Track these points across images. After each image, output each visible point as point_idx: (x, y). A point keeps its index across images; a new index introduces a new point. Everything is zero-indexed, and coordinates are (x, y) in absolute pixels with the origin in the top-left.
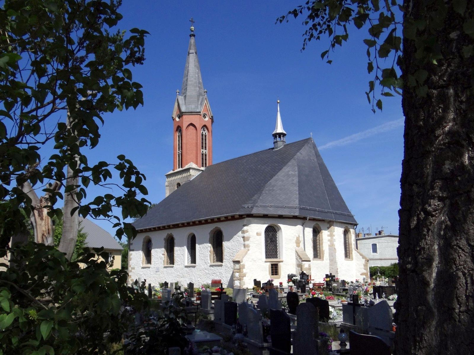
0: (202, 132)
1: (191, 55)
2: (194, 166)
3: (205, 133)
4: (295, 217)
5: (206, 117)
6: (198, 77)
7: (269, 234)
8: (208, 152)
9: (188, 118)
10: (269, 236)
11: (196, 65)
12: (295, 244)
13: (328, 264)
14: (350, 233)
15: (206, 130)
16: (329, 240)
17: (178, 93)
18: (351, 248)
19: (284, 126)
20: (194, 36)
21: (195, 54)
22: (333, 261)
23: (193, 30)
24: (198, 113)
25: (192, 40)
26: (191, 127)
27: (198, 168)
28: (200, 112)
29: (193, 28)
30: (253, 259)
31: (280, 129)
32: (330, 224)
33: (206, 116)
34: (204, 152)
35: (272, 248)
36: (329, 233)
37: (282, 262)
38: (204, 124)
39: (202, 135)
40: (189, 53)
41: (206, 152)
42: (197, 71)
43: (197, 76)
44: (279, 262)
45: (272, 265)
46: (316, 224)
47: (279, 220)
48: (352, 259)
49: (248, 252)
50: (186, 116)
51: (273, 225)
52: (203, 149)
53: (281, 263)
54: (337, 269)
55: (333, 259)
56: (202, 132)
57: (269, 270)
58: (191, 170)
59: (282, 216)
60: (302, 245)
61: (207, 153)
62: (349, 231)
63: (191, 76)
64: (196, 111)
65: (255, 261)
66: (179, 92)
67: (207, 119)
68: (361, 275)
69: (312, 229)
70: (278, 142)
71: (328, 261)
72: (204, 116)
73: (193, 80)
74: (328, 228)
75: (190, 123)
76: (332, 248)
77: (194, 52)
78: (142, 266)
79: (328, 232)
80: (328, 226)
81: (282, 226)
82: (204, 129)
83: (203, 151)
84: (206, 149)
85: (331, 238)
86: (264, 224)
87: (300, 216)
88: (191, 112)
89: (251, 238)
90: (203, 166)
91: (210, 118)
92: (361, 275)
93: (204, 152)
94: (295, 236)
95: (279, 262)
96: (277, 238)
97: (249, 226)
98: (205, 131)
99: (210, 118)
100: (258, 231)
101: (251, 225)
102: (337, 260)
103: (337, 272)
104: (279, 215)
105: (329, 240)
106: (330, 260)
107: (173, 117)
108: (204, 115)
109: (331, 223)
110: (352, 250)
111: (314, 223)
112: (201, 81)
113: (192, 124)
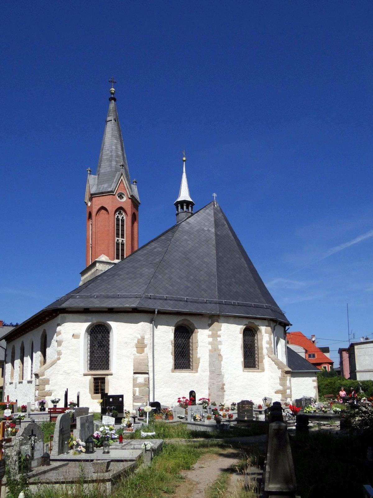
0: (118, 216)
1: (109, 123)
2: (104, 258)
3: (123, 217)
4: (135, 311)
5: (123, 197)
6: (117, 148)
7: (97, 336)
8: (126, 241)
9: (98, 200)
10: (97, 338)
11: (113, 134)
12: (135, 349)
13: (207, 378)
14: (261, 332)
15: (124, 214)
16: (210, 343)
17: (89, 172)
18: (262, 353)
19: (192, 192)
20: (115, 99)
21: (113, 121)
22: (216, 372)
23: (113, 92)
24: (111, 193)
25: (112, 104)
26: (103, 211)
27: (110, 261)
28: (112, 192)
29: (113, 89)
30: (65, 372)
31: (184, 195)
32: (211, 319)
33: (124, 196)
34: (120, 241)
35: (99, 353)
36: (210, 333)
37: (112, 375)
38: (119, 206)
39: (118, 220)
40: (107, 122)
41: (123, 241)
42: (116, 141)
43: (114, 147)
44: (107, 375)
45: (95, 379)
46: (183, 320)
47: (109, 315)
48: (263, 370)
49: (58, 362)
50: (96, 198)
51: (252, 327)
52: (118, 235)
53: (109, 377)
54: (224, 385)
55: (215, 370)
56: (116, 216)
57: (90, 387)
58: (97, 264)
59: (180, 312)
60: (148, 350)
61: (125, 242)
62: (258, 329)
63: (107, 148)
64: (107, 191)
65: (68, 374)
66: (90, 171)
67: (125, 199)
68: (276, 393)
69: (173, 328)
70: (179, 214)
71: (208, 373)
72: (121, 196)
73: (108, 154)
74: (210, 325)
75: (100, 206)
76: (216, 356)
77: (113, 119)
78: (10, 381)
79: (209, 331)
80: (210, 322)
81: (112, 324)
82: (121, 212)
83: (118, 240)
84: (123, 236)
85: (213, 340)
86: (85, 322)
87: (140, 309)
88: (102, 193)
89: (63, 342)
90: (118, 258)
91: (129, 198)
92: (276, 393)
93: (120, 241)
94: (135, 337)
95: (107, 375)
96: (109, 341)
97: (63, 325)
98: (122, 214)
99: (129, 198)
100: (76, 332)
101: (66, 324)
102: (223, 371)
103: (223, 388)
104: (132, 309)
105: (210, 343)
106: (210, 371)
107: (86, 203)
108: (121, 195)
109: (215, 318)
110: (263, 358)
111: (177, 320)
112: (120, 153)
113: (103, 208)
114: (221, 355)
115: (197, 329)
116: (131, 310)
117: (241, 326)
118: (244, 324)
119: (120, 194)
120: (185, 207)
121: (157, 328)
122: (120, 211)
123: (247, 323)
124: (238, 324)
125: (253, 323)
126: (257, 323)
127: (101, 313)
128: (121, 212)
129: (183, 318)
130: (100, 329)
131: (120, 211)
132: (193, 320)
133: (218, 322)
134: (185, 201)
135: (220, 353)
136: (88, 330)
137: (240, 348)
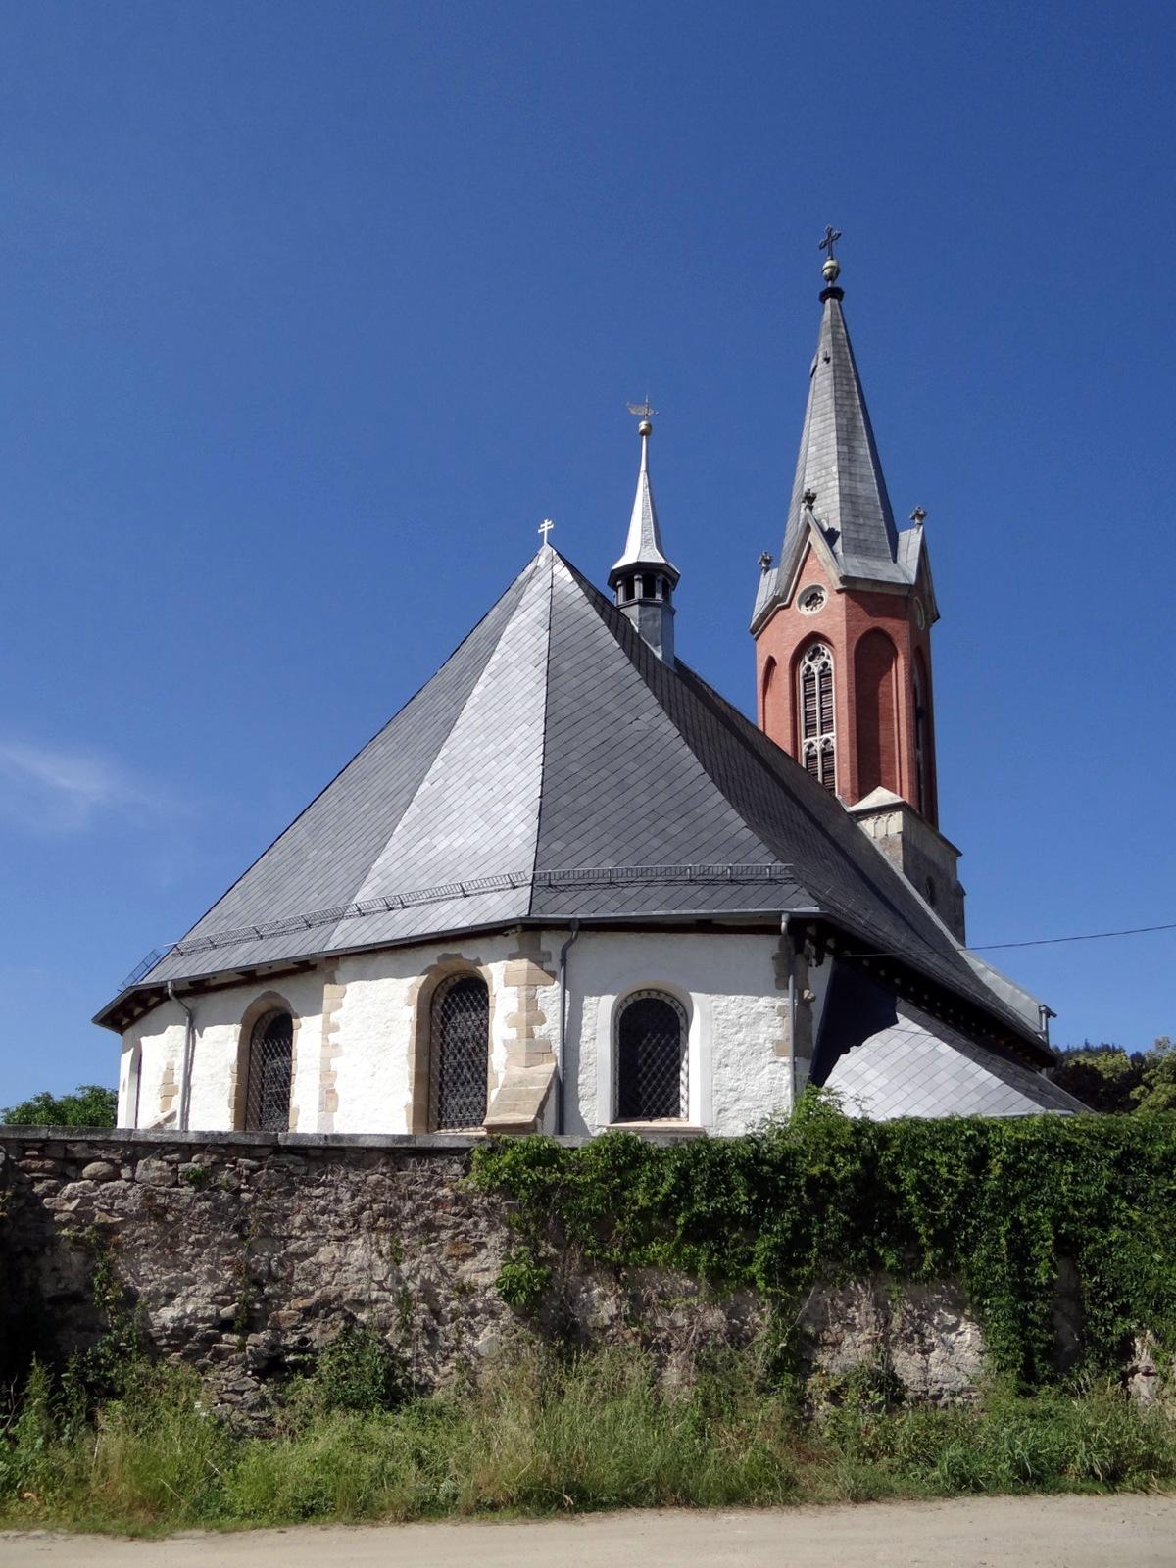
38: (804, 632)
46: (264, 996)
104: (191, 983)
111: (246, 999)
114: (333, 1091)
115: (297, 1018)
116: (241, 977)
117: (412, 980)
118: (422, 970)
119: (812, 593)
120: (638, 588)
121: (201, 1036)
122: (814, 646)
123: (436, 963)
124: (399, 975)
125: (459, 956)
126: (468, 952)
127: (644, 924)
128: (819, 648)
129: (263, 991)
130: (468, 998)
131: (814, 646)
132: (289, 992)
133: (333, 981)
134: (638, 567)
135: (332, 1085)
136: (433, 1003)
137: (404, 1058)
